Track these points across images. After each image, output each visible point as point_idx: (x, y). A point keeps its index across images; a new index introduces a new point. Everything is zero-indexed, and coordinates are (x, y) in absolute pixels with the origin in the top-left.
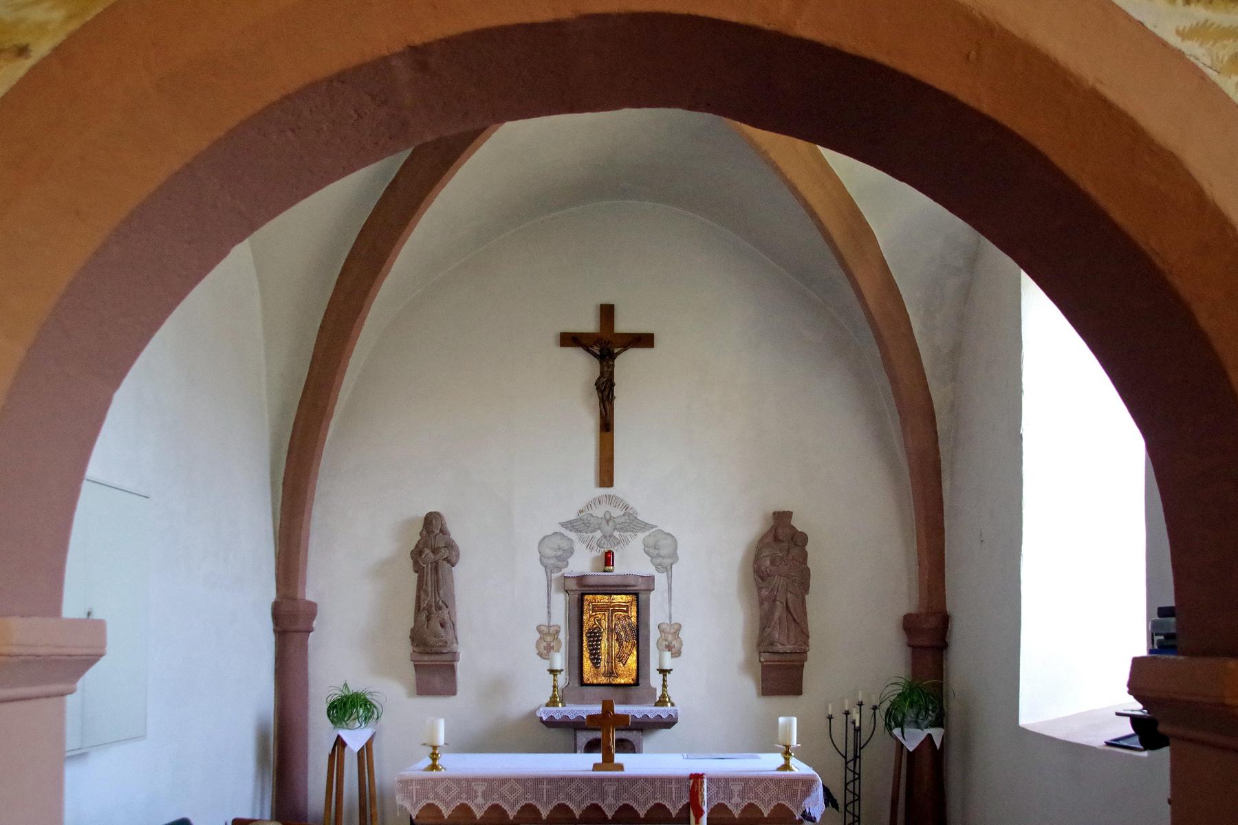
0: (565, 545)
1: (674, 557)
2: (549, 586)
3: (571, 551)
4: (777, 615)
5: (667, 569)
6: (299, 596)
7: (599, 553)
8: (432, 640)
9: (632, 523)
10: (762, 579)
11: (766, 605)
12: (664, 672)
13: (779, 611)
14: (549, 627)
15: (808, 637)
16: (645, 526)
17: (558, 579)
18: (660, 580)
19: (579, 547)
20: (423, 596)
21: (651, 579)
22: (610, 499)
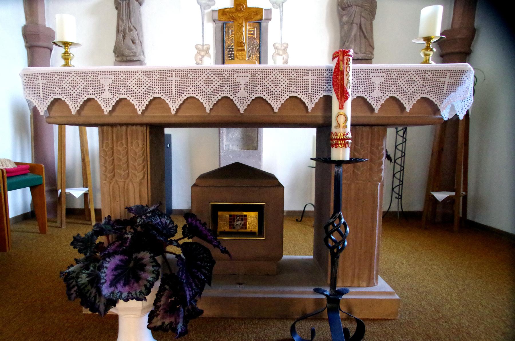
2: (203, 18)
4: (353, 34)
5: (280, 6)
6: (40, 22)
8: (127, 52)
10: (343, 9)
11: (346, 27)
13: (355, 29)
14: (203, 45)
15: (373, 49)
17: (209, 13)
18: (275, 14)
20: (120, 23)
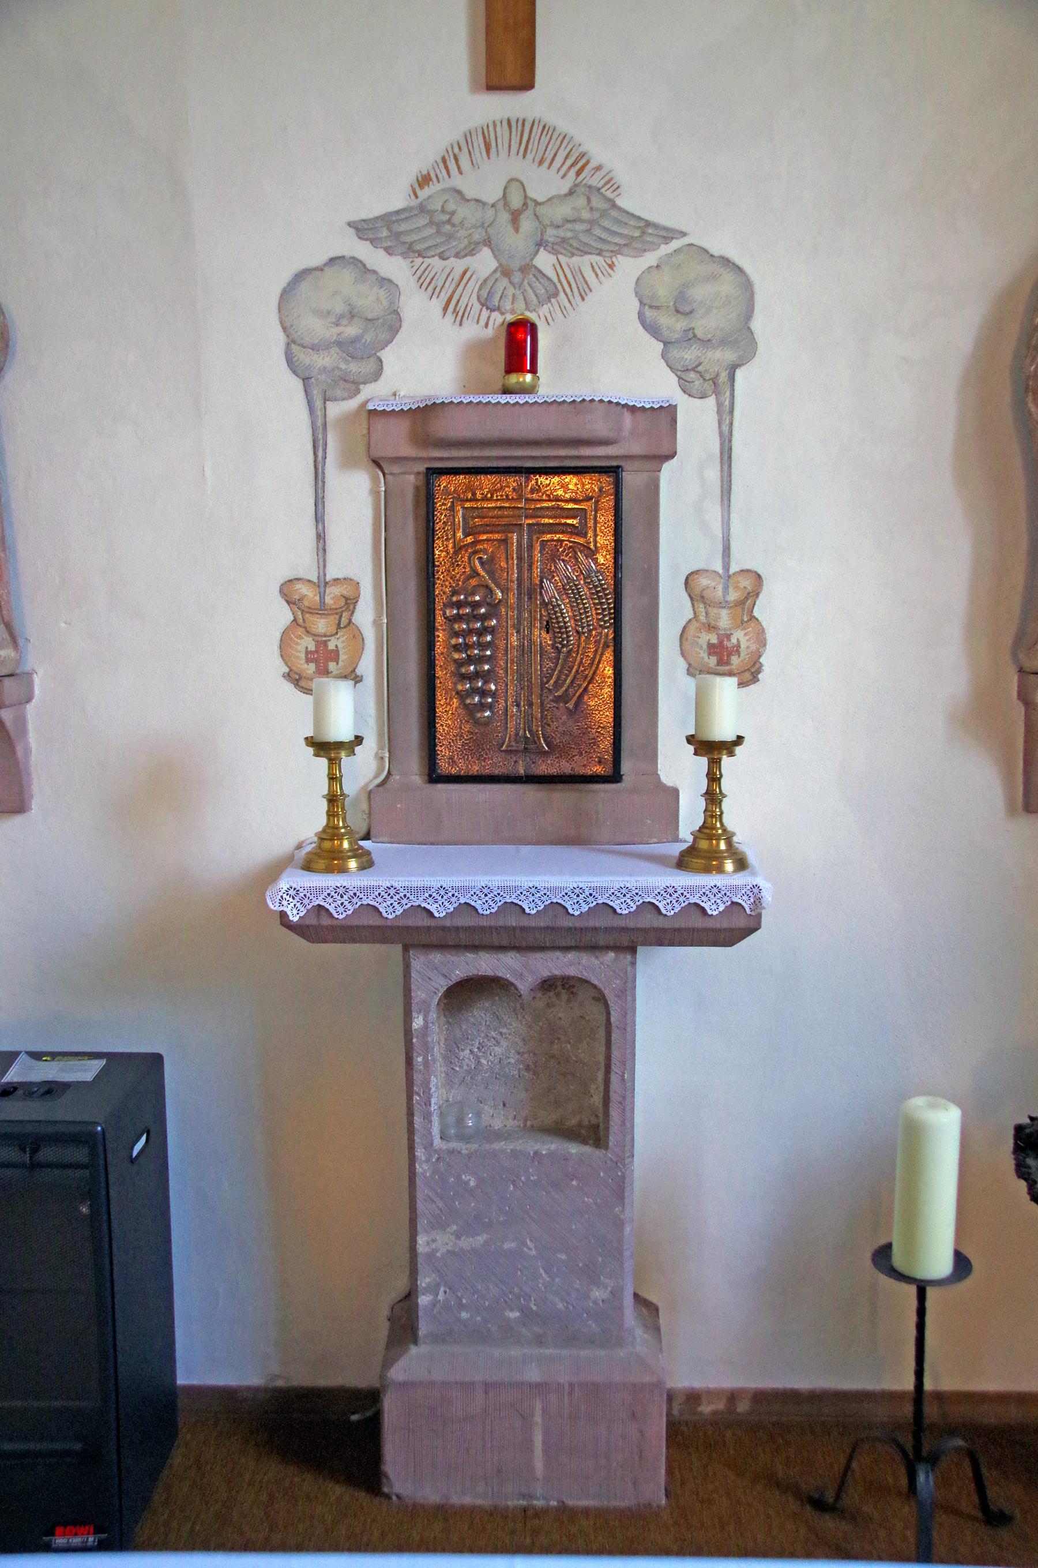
0: (370, 300)
1: (742, 342)
3: (391, 324)
5: (719, 386)
7: (487, 327)
9: (601, 225)
12: (711, 750)
16: (647, 233)
19: (418, 308)
21: (665, 416)
22: (527, 135)
